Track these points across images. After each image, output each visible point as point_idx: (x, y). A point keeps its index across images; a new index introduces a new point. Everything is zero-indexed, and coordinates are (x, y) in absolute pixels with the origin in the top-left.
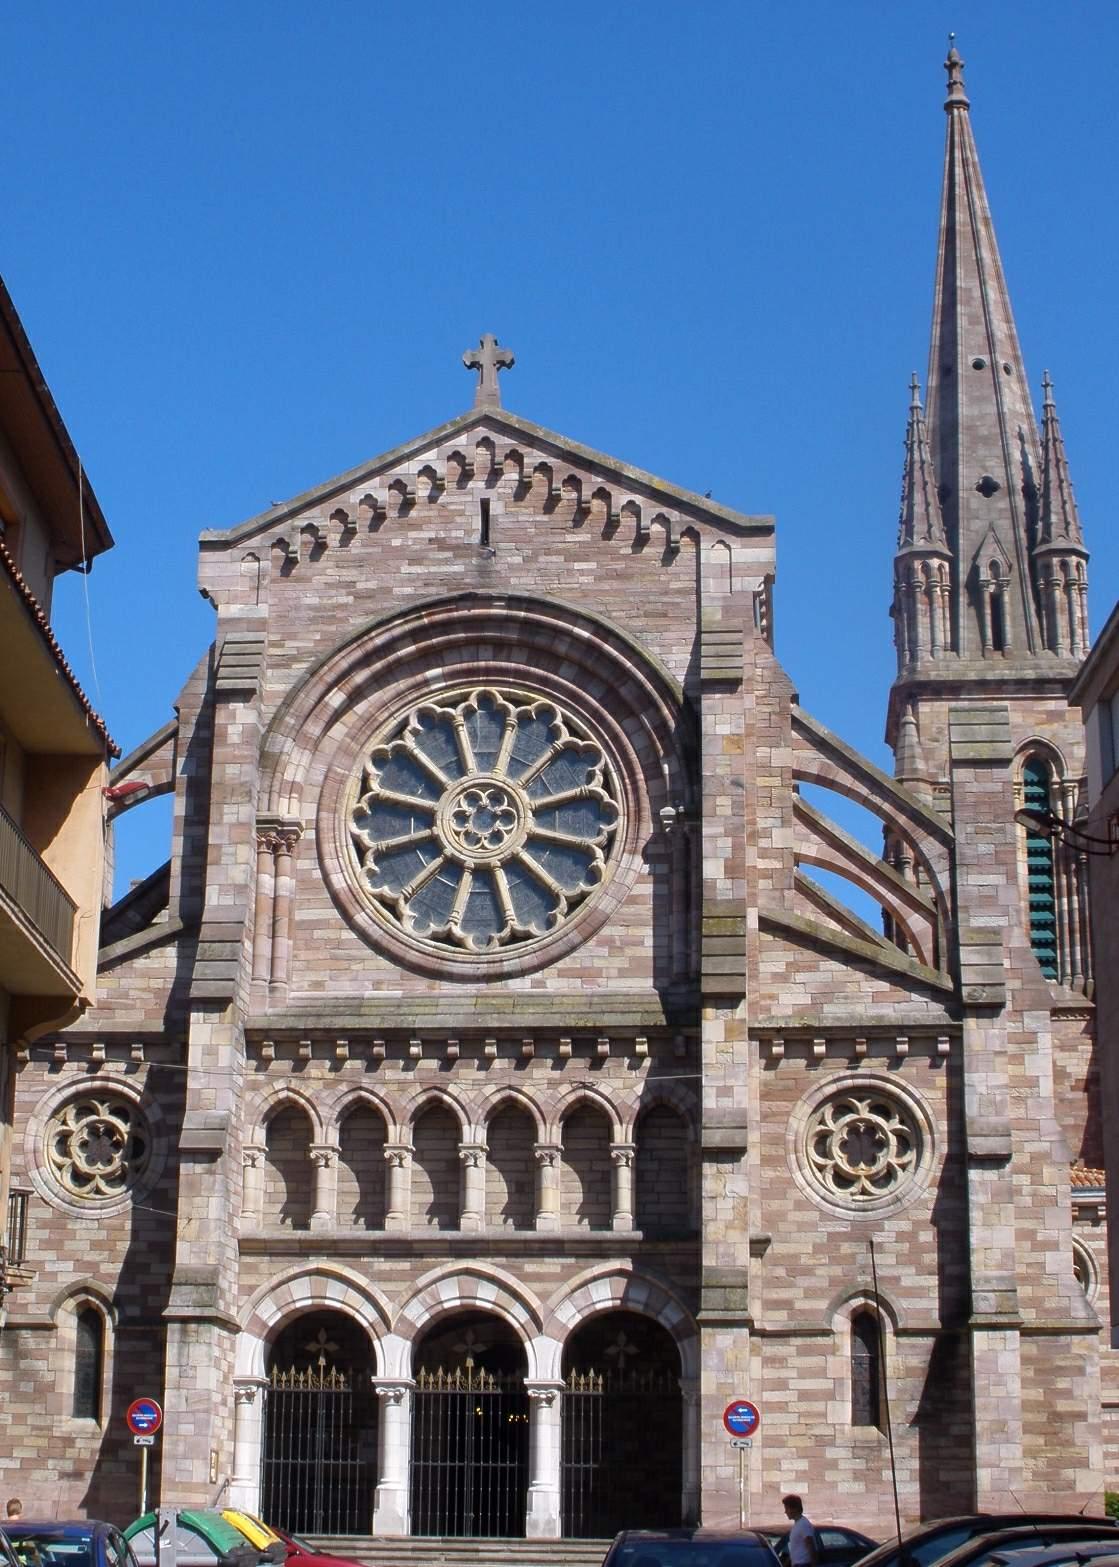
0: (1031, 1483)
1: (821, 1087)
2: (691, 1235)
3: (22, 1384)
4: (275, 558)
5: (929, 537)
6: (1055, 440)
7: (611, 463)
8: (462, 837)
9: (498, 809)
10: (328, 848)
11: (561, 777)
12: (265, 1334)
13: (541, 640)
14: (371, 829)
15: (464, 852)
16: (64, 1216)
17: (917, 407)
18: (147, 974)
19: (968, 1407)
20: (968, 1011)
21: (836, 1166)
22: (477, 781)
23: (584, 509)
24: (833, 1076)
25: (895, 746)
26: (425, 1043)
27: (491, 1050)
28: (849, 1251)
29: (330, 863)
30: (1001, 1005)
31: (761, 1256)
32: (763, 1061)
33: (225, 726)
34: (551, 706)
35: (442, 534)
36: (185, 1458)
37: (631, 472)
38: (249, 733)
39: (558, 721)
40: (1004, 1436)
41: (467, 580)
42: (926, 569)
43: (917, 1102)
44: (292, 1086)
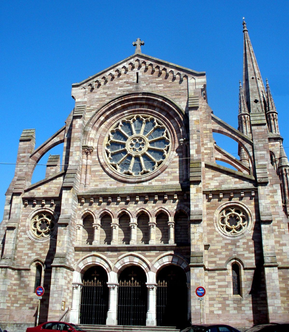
0: (283, 311)
1: (222, 206)
2: (188, 244)
3: (22, 284)
4: (89, 88)
5: (245, 111)
6: (269, 91)
7: (166, 62)
8: (132, 149)
9: (141, 143)
10: (100, 153)
11: (156, 135)
12: (80, 271)
13: (150, 103)
14: (111, 149)
15: (132, 153)
16: (34, 242)
17: (241, 86)
18: (56, 184)
19: (264, 289)
20: (259, 185)
21: (226, 226)
22: (135, 136)
23: (160, 72)
24: (225, 203)
25: (240, 156)
26: (121, 198)
27: (138, 199)
28: (231, 248)
29: (100, 157)
30: (267, 183)
31: (208, 250)
32: (207, 200)
33: (75, 124)
34: (153, 118)
35: (127, 81)
36: (55, 303)
37: (171, 64)
38: (81, 126)
39: (155, 121)
40: (275, 297)
41: (133, 90)
42: (245, 117)
43: (247, 209)
44: (89, 209)
